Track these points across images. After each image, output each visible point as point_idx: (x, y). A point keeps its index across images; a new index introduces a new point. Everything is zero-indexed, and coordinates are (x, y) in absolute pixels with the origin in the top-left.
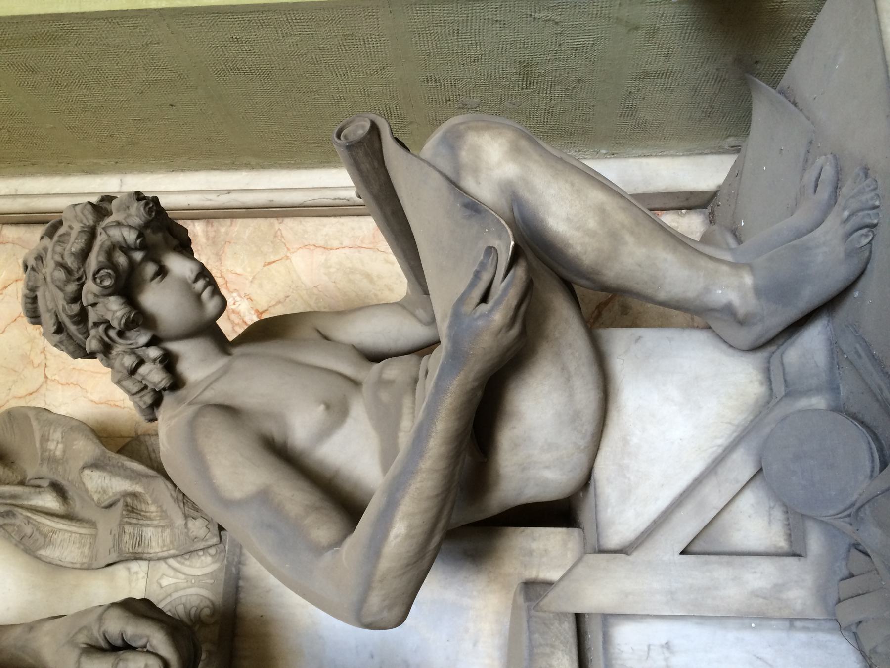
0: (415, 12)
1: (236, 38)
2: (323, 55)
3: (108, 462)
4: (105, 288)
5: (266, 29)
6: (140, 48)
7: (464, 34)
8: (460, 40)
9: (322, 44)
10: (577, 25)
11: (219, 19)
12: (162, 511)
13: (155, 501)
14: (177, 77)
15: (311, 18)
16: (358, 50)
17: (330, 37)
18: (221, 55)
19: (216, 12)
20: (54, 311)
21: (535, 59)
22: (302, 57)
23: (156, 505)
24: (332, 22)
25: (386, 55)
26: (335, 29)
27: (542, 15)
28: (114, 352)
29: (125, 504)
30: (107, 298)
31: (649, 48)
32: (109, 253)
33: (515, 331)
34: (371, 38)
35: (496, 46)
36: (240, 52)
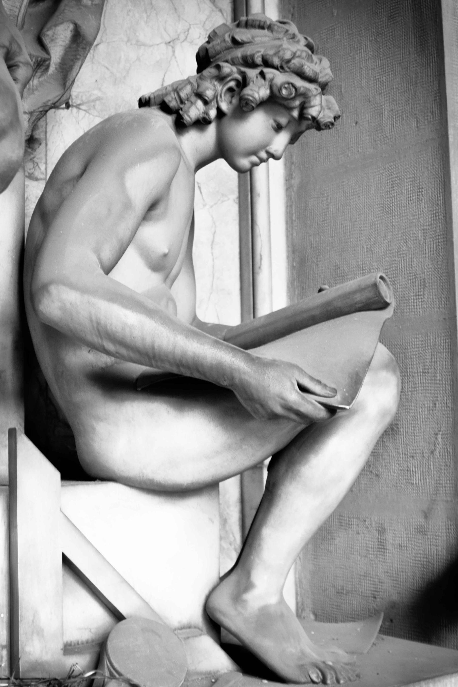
0: (444, 338)
1: (422, 191)
2: (406, 260)
3: (81, 47)
4: (280, 90)
5: (430, 217)
6: (413, 111)
7: (424, 378)
8: (419, 374)
9: (416, 260)
10: (431, 469)
11: (439, 181)
12: (33, 90)
13: (41, 83)
14: (385, 135)
15: (440, 255)
16: (411, 290)
17: (423, 267)
18: (406, 176)
19: (446, 180)
20: (253, 41)
21: (400, 437)
22: (404, 242)
23: (38, 85)
24: (436, 271)
25: (406, 313)
26: (430, 273)
27: (440, 440)
28: (216, 83)
29: (46, 59)
30: (269, 88)
31: (408, 530)
32: (299, 94)
33: (279, 410)
34: (422, 301)
35: (413, 404)
36: (410, 192)
